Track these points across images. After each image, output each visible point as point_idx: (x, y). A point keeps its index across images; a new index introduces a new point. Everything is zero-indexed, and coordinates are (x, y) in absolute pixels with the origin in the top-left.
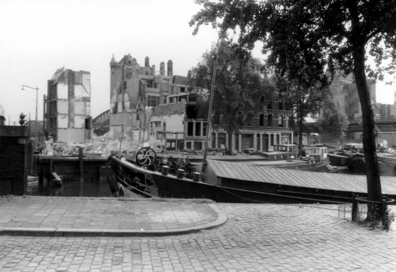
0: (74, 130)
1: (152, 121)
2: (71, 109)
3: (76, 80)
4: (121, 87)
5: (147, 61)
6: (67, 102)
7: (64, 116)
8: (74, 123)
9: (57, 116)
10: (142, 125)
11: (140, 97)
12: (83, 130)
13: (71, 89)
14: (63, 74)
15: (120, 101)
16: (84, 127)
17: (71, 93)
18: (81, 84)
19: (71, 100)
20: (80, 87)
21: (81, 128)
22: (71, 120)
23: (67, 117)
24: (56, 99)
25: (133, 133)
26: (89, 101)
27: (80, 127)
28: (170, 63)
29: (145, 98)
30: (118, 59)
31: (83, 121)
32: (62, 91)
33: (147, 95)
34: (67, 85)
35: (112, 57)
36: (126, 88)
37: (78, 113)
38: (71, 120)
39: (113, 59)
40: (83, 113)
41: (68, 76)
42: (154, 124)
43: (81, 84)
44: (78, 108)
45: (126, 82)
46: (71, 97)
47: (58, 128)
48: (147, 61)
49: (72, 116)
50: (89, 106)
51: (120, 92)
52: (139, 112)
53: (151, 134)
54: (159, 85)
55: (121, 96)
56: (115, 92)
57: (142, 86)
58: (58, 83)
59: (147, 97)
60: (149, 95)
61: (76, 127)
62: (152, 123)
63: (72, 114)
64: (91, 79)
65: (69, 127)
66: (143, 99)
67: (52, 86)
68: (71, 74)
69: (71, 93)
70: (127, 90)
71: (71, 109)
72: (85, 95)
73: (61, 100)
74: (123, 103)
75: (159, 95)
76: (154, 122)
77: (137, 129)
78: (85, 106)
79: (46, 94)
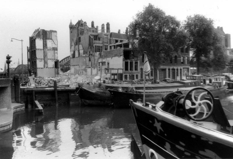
0: (48, 69)
2: (45, 56)
3: (48, 36)
4: (77, 41)
5: (93, 23)
6: (43, 51)
8: (47, 65)
9: (36, 60)
12: (54, 69)
14: (39, 32)
15: (77, 50)
16: (54, 67)
17: (45, 45)
18: (51, 39)
19: (45, 50)
20: (51, 41)
21: (52, 68)
22: (46, 63)
24: (35, 49)
25: (87, 70)
26: (57, 50)
27: (52, 67)
28: (108, 25)
29: (93, 47)
30: (74, 23)
31: (53, 63)
32: (39, 44)
33: (94, 45)
34: (42, 40)
38: (46, 63)
39: (71, 23)
40: (53, 58)
41: (43, 34)
43: (51, 39)
45: (80, 38)
47: (37, 68)
48: (93, 23)
49: (46, 59)
51: (77, 44)
52: (90, 56)
55: (77, 46)
56: (73, 44)
58: (36, 39)
59: (94, 46)
60: (95, 45)
62: (99, 63)
63: (46, 59)
64: (57, 35)
66: (92, 48)
69: (45, 45)
70: (81, 42)
71: (45, 56)
72: (54, 46)
75: (102, 45)
77: (90, 67)
78: (54, 53)
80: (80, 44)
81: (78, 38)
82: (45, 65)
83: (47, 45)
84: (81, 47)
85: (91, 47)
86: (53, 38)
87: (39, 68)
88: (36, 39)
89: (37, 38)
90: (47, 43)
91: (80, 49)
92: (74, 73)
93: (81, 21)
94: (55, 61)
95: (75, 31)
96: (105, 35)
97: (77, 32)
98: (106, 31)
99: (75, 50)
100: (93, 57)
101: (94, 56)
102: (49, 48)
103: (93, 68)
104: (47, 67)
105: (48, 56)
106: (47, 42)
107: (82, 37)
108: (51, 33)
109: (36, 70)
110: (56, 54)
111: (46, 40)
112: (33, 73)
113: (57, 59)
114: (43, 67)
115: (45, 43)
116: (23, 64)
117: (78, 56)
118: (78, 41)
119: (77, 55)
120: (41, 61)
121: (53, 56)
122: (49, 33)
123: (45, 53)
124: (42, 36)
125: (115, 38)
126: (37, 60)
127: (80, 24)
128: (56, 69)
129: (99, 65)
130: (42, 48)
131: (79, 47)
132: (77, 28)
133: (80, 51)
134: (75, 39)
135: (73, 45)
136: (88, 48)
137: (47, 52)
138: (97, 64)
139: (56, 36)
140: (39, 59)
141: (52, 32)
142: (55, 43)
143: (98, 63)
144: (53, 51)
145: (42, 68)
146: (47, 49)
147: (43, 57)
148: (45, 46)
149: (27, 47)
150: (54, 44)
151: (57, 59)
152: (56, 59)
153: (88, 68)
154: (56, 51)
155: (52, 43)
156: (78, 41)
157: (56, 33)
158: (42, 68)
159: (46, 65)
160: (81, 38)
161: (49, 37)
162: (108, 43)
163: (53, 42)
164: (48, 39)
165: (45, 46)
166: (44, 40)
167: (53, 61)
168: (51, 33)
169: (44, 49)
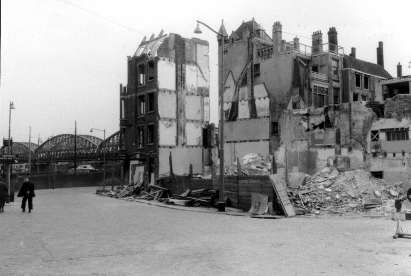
0: (185, 149)
1: (374, 128)
2: (180, 110)
3: (187, 55)
4: (246, 75)
5: (277, 27)
6: (174, 96)
7: (169, 123)
8: (184, 137)
9: (158, 123)
10: (342, 138)
11: (298, 90)
12: (200, 149)
13: (179, 72)
14: (166, 41)
15: (243, 99)
16: (202, 143)
17: (180, 79)
18: (196, 64)
19: (179, 93)
20: (194, 68)
21: (197, 146)
22: (180, 131)
23: (175, 124)
24: (155, 90)
25: (317, 153)
26: (208, 96)
27: (196, 144)
28: (333, 34)
29: (310, 90)
30: (230, 30)
31: (199, 133)
32: (166, 73)
33: (313, 84)
34: (174, 64)
35: (221, 24)
36: (258, 75)
37: (192, 118)
38: (180, 131)
39: (222, 29)
40: (199, 118)
41: (175, 48)
42: (383, 136)
43: (196, 64)
44: (192, 107)
45: (257, 66)
46: (180, 87)
47: (159, 146)
48: (277, 27)
49: (181, 121)
50: (208, 104)
51: (244, 83)
52: (330, 113)
53: (375, 155)
54: (326, 68)
55: (245, 90)
56: (230, 82)
57: (302, 70)
58: (157, 59)
59: (312, 87)
60: (315, 84)
61: (188, 144)
62: (375, 132)
63: (182, 119)
64: (209, 54)
65: (177, 145)
66: (306, 92)
67: (142, 67)
68: (180, 45)
69: (180, 79)
70: (262, 78)
71: (180, 110)
72: (202, 84)
73: (164, 91)
74: (252, 102)
75: (327, 87)
76: (383, 130)
77: (329, 147)
78: (203, 105)
79: (125, 84)
80: (258, 84)
81: (249, 67)
82: (179, 136)
83: (184, 80)
84: (260, 91)
85: (300, 90)
86: (198, 62)
87: (164, 147)
88: (159, 59)
89: (162, 58)
90: (184, 74)
91: (256, 95)
92: (284, 164)
93: (254, 24)
94: (203, 126)
95: (240, 50)
96: (333, 59)
97: (245, 52)
98: (325, 48)
99: (238, 99)
100: (343, 116)
101: (349, 112)
102: (189, 90)
103: (343, 146)
104: (183, 145)
105: (186, 110)
106: (185, 70)
107: (265, 65)
108: (196, 46)
109: (156, 151)
110: (206, 108)
111: (183, 65)
112: (140, 160)
113: (208, 122)
114: (173, 143)
115: (179, 72)
116: (31, 142)
117: (248, 116)
118: (249, 76)
119: (244, 110)
120: (170, 125)
121: (199, 111)
122: (191, 46)
123: (179, 102)
124: (174, 52)
125: (356, 69)
126: (160, 122)
127: (249, 30)
128: (206, 150)
129: (375, 140)
130: (172, 87)
131: (252, 90)
132: (246, 40)
133: (257, 103)
134: (238, 70)
135: (229, 87)
136: (291, 93)
137: (186, 100)
138: (365, 135)
139: (208, 56)
140: (164, 119)
141: (199, 44)
142: (203, 77)
143: (370, 134)
144: (199, 98)
145: (170, 147)
146: (185, 92)
147: (174, 116)
148: (179, 81)
149: (119, 86)
150: (202, 78)
151: (208, 122)
152: (205, 120)
153: (321, 147)
154: (206, 99)
155: (197, 76)
156: (249, 76)
157: (207, 47)
158: (170, 147)
159: (181, 138)
160: (261, 66)
161: (191, 55)
162: (338, 81)
163: (199, 72)
164: (189, 62)
165: (179, 81)
166: (179, 66)
167: (200, 127)
168: (194, 45)
169: (176, 92)
